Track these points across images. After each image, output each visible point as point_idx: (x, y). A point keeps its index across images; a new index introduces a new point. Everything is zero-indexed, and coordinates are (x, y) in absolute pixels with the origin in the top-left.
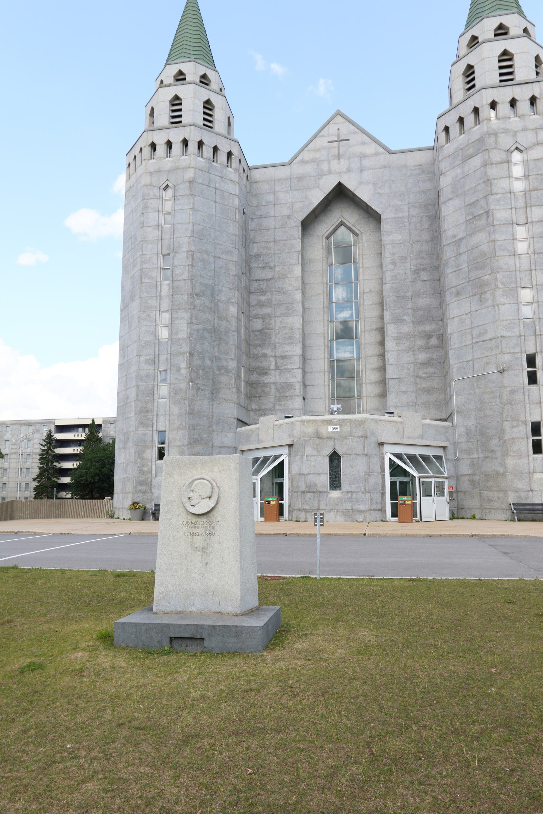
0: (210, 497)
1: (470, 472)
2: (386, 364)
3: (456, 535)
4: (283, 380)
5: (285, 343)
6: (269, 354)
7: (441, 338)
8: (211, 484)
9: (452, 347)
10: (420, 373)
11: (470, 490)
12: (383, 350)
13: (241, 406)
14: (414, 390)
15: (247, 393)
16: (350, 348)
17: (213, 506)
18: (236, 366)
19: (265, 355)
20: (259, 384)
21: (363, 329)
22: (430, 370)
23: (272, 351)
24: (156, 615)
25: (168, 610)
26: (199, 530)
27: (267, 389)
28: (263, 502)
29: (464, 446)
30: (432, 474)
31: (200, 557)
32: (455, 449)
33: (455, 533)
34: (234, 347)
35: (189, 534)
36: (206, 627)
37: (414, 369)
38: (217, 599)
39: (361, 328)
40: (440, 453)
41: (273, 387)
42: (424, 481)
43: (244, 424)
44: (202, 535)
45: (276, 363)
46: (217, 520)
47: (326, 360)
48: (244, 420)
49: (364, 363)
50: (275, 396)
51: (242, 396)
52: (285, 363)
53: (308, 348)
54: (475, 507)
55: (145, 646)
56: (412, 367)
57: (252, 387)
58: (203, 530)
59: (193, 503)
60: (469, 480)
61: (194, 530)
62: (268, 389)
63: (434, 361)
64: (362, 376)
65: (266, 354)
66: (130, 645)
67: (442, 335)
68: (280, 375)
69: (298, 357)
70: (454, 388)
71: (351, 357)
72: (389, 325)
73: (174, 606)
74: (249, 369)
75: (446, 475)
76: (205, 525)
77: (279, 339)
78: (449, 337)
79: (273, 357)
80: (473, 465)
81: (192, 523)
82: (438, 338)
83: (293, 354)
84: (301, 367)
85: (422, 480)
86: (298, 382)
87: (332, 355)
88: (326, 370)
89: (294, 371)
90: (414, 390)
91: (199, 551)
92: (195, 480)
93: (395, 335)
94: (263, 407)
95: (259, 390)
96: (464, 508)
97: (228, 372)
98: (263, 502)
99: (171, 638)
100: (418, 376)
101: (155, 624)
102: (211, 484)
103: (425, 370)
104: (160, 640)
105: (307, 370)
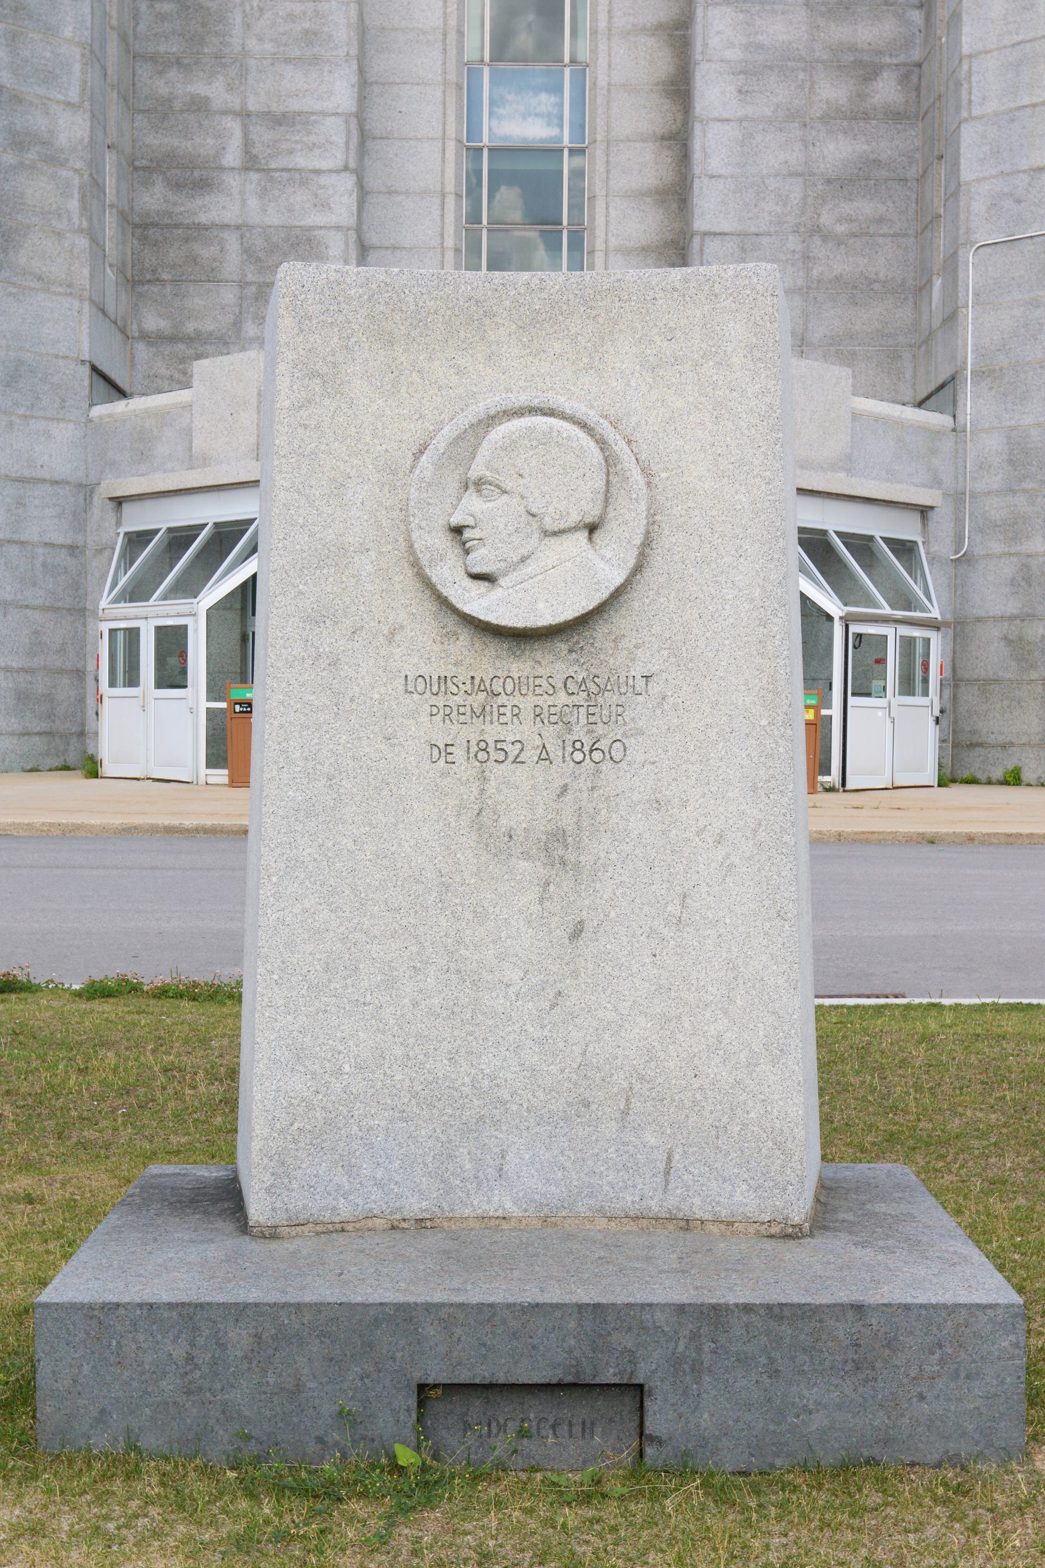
0: (592, 529)
1: (1012, 607)
2: (697, 170)
3: (1030, 836)
4: (274, 218)
5: (287, 60)
6: (217, 104)
7: (914, 79)
8: (602, 444)
9: (976, 112)
10: (827, 219)
11: (1008, 676)
12: (680, 117)
13: (103, 312)
14: (800, 282)
15: (124, 265)
16: (546, 101)
17: (618, 579)
18: (86, 134)
19: (200, 106)
20: (176, 226)
21: (602, 24)
22: (866, 208)
23: (230, 88)
24: (274, 1245)
25: (345, 1210)
26: (526, 730)
27: (206, 252)
28: (223, 705)
29: (996, 508)
30: (887, 610)
31: (533, 894)
32: (959, 521)
33: (1025, 830)
34: (76, 53)
35: (459, 753)
36: (660, 1317)
37: (805, 198)
38: (651, 1139)
39: (594, 20)
40: (907, 529)
41: (233, 243)
42: (859, 636)
43: (113, 392)
44: (544, 757)
45: (247, 144)
46: (637, 670)
47: (451, 146)
48: (114, 375)
49: (600, 167)
50: (243, 284)
51: (108, 271)
52: (284, 146)
53: (376, 89)
54: (1024, 739)
55: (254, 1448)
56: (795, 191)
57: (144, 239)
58: (549, 731)
59: (481, 560)
60: (1005, 638)
61: (492, 732)
62: (214, 249)
63: (884, 173)
64: (592, 218)
65: (207, 99)
66: (149, 1441)
67: (919, 65)
68: (263, 193)
69: (339, 121)
70: (971, 277)
71: (551, 139)
72: (715, 12)
73: (379, 1184)
74: (131, 162)
75: (935, 613)
76: (562, 698)
77: (261, 39)
78: (965, 67)
79: (237, 114)
80: (1028, 581)
81: (477, 685)
82: (904, 79)
83: (318, 106)
84: (352, 165)
85: (854, 629)
86: (338, 228)
87: (473, 128)
88: (450, 187)
89: (323, 180)
90: (800, 282)
91: (526, 855)
92: (491, 420)
93: (734, 54)
94: (190, 327)
95: (174, 253)
96: (980, 745)
97: (54, 159)
98: (223, 705)
99: (422, 1388)
100: (816, 230)
101: (317, 1308)
102: (602, 444)
103: (847, 208)
104: (353, 1407)
105: (372, 182)
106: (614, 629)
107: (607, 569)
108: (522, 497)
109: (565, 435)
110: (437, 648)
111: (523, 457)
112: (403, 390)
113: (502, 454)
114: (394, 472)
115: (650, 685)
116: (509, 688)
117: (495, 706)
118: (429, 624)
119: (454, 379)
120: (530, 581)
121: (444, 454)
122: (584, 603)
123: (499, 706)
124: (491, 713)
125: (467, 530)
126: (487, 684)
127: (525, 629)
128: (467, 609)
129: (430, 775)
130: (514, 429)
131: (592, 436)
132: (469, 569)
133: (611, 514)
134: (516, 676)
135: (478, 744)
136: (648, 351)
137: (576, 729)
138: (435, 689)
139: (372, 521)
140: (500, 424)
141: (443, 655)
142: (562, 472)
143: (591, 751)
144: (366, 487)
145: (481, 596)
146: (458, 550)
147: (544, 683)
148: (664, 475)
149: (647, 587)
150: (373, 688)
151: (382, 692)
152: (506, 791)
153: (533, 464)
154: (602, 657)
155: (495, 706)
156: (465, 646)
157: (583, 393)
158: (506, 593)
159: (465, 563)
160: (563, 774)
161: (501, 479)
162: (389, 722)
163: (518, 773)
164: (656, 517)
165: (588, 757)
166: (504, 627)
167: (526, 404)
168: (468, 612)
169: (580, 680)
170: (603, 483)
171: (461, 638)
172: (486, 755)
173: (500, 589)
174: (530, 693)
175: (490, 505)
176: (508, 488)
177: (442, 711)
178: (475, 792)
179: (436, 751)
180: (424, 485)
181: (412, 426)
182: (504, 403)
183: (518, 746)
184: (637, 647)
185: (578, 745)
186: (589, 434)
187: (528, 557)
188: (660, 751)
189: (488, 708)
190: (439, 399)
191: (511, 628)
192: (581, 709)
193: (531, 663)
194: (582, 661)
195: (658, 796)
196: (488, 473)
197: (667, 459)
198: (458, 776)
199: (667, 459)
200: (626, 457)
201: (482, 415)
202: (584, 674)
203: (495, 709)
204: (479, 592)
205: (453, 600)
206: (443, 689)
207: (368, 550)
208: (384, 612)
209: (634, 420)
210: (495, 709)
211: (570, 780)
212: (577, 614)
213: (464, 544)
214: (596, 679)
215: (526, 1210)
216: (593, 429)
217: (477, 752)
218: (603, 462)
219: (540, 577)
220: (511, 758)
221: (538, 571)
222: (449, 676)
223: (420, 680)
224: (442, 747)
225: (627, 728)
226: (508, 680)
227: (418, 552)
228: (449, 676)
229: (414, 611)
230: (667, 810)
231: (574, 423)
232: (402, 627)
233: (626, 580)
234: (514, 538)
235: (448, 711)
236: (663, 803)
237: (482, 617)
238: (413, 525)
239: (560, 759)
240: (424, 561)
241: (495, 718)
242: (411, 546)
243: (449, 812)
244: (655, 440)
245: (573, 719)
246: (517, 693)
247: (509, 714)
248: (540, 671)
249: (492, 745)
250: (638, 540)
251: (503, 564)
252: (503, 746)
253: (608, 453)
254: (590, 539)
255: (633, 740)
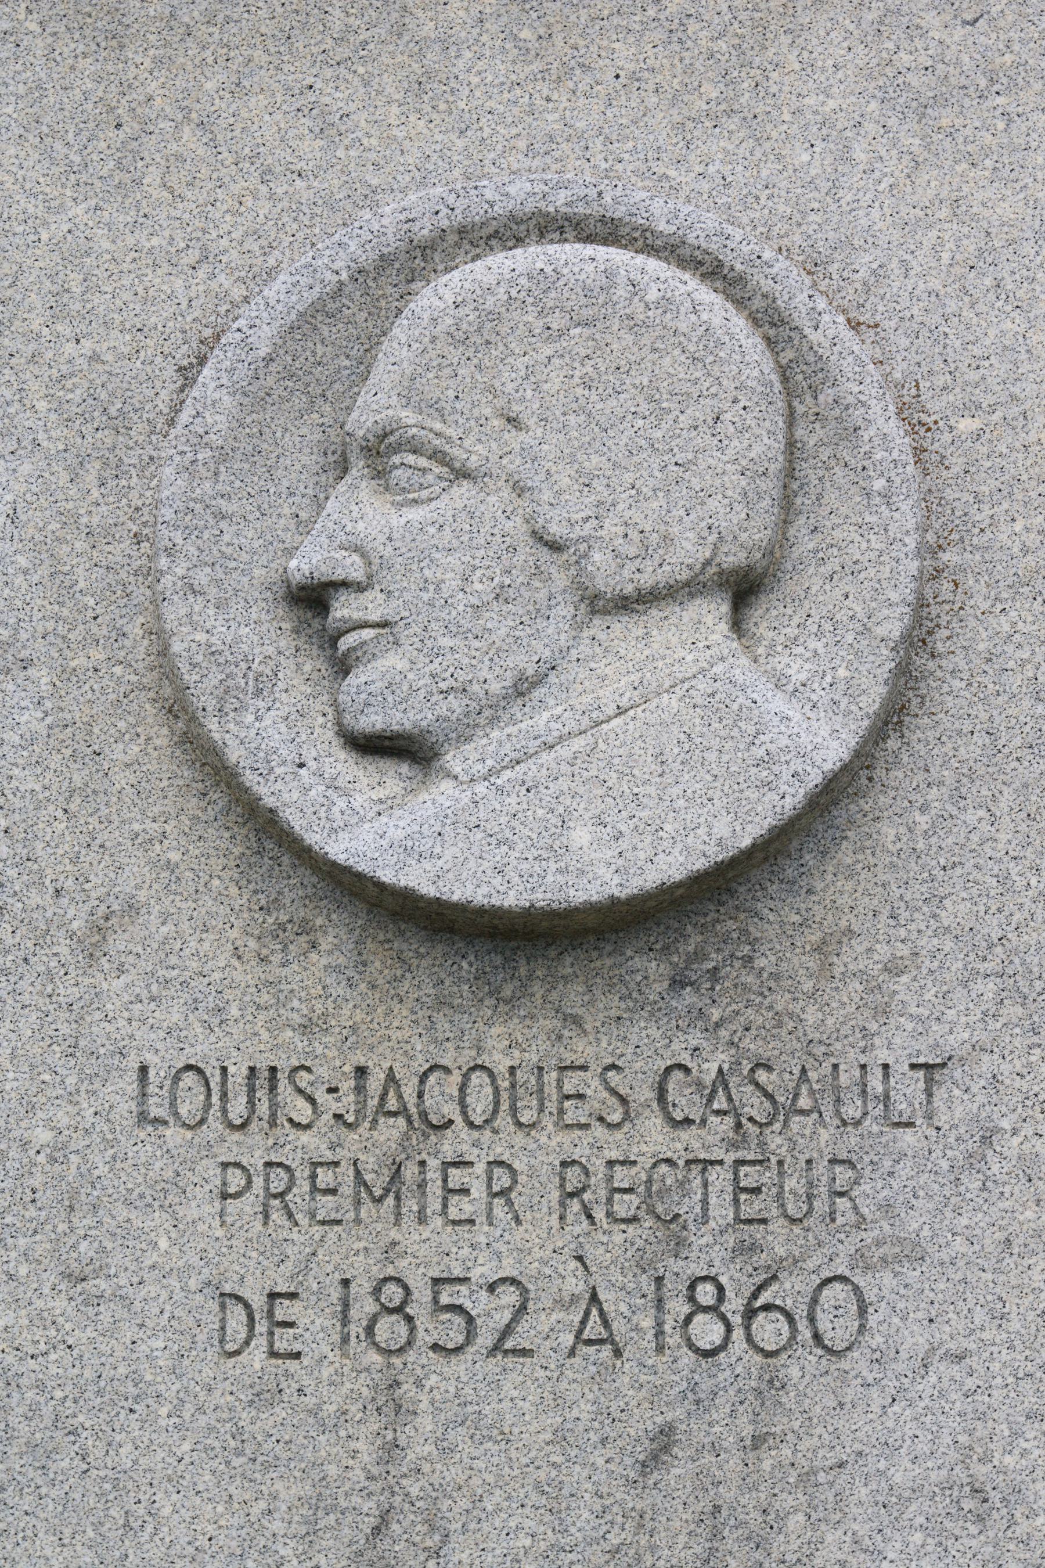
106: (818, 911)
107: (796, 716)
108: (519, 489)
109: (652, 295)
110: (245, 975)
111: (521, 363)
112: (152, 177)
113: (454, 355)
114: (119, 423)
115: (940, 1094)
116: (479, 1105)
117: (433, 1163)
118: (220, 898)
119: (311, 148)
120: (545, 757)
121: (269, 360)
122: (722, 828)
123: (446, 1165)
124: (422, 1185)
125: (343, 596)
126: (409, 1092)
127: (529, 914)
128: (338, 850)
129: (217, 1398)
130: (490, 279)
131: (740, 303)
132: (347, 719)
133: (805, 544)
134: (501, 1064)
135: (377, 1291)
136: (905, 58)
137: (700, 1239)
138: (238, 1109)
139: (44, 571)
140: (448, 270)
141: (265, 998)
142: (644, 408)
143: (750, 1314)
144: (26, 468)
145: (385, 806)
146: (314, 663)
147: (594, 1087)
148: (966, 425)
149: (921, 776)
150: (31, 1109)
151: (63, 1120)
152: (467, 1448)
153: (555, 383)
154: (781, 1001)
155: (433, 1163)
156: (337, 969)
157: (705, 186)
158: (466, 798)
159: (335, 704)
160: (657, 1391)
161: (451, 432)
162: (82, 1222)
163: (508, 1389)
164: (945, 557)
165: (738, 1334)
166: (462, 908)
167: (529, 208)
168: (341, 859)
169: (709, 1078)
170: (778, 445)
171: (326, 943)
172: (403, 1330)
173: (447, 785)
174: (548, 1122)
175: (414, 514)
176: (474, 462)
177: (258, 1182)
178: (367, 1452)
179: (237, 1317)
180: (204, 455)
181: (178, 283)
182: (460, 205)
183: (509, 1296)
184: (893, 969)
185: (706, 1294)
186: (729, 297)
187: (539, 680)
188: (980, 1316)
189: (410, 1171)
190: (264, 208)
191: (481, 911)
192: (713, 1174)
193: (549, 1023)
194: (716, 1014)
195: (981, 1471)
196: (408, 416)
197: (973, 376)
198: (310, 1401)
199: (973, 376)
200: (848, 364)
201: (392, 242)
202: (723, 1058)
203: (433, 1174)
204: (381, 793)
205: (295, 821)
206: (263, 1108)
207: (26, 664)
208: (75, 860)
209: (865, 262)
210: (433, 1174)
211: (679, 1413)
212: (700, 864)
213: (334, 641)
214: (762, 1076)
215: (644, 711)
216: (741, 280)
217: (374, 1320)
218: (774, 378)
219: (579, 743)
220: (485, 1339)
221: (572, 725)
222: (284, 1064)
223: (189, 1079)
224: (258, 1302)
225: (869, 1237)
226: (476, 1078)
227: (184, 668)
228: (284, 1064)
229: (174, 856)
230: (1012, 1523)
231: (683, 263)
232: (132, 908)
233: (857, 754)
234: (490, 619)
235: (278, 1181)
236: (995, 1497)
237: (386, 876)
238: (167, 581)
239: (648, 1341)
240: (204, 698)
241: (434, 1205)
242: (164, 652)
243: (277, 1526)
244: (936, 319)
245: (689, 1207)
246: (503, 1121)
247: (478, 1191)
248: (582, 1049)
249: (422, 1294)
250: (893, 628)
251: (456, 704)
252: (462, 1296)
253: (789, 354)
254: (737, 625)
255: (887, 1279)
